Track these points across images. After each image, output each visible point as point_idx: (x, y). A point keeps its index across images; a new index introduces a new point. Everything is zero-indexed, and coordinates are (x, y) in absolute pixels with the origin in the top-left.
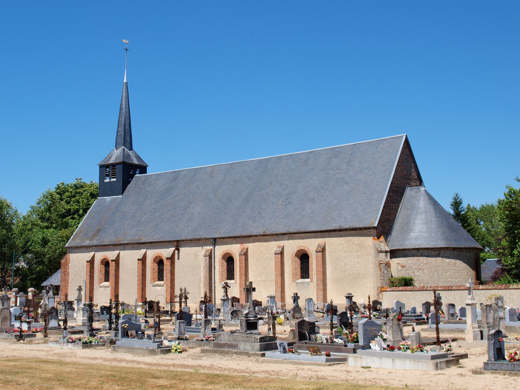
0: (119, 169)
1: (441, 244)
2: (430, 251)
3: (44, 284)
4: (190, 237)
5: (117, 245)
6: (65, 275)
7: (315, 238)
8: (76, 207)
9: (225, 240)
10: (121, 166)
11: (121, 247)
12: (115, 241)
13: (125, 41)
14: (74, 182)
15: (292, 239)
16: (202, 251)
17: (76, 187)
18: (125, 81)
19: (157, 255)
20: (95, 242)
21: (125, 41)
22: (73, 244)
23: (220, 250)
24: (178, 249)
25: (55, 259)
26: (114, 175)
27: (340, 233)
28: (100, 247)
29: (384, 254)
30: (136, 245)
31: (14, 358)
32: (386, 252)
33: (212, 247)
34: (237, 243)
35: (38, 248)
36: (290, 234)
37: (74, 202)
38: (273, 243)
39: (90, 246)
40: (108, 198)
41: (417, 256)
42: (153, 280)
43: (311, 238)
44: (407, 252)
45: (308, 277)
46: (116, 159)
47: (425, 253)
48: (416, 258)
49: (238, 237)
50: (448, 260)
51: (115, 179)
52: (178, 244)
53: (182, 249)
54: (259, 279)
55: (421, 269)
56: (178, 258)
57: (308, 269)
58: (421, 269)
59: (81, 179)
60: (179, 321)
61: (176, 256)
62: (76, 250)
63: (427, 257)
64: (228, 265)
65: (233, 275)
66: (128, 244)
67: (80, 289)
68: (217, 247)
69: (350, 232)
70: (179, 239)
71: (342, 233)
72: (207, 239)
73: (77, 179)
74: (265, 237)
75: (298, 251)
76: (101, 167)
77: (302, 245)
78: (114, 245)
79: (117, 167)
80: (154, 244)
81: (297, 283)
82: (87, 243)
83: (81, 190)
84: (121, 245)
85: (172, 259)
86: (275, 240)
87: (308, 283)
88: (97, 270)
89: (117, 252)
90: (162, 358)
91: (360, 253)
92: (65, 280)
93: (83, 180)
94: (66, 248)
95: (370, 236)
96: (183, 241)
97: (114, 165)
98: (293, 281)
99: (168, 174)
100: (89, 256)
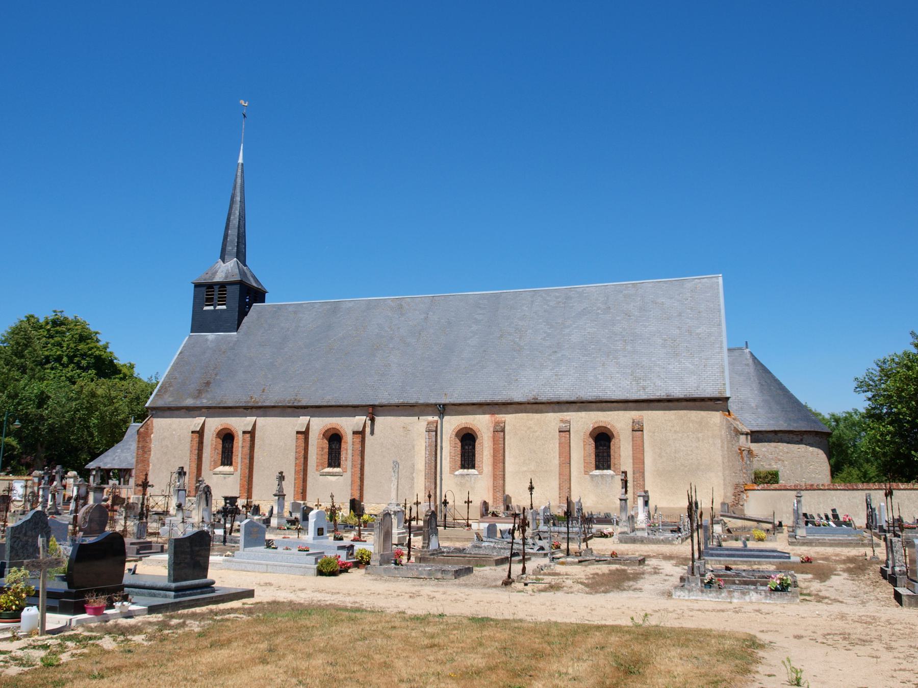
0: (233, 293)
1: (782, 426)
2: (791, 436)
3: (92, 465)
4: (395, 401)
5: (252, 408)
6: (144, 452)
7: (625, 409)
8: (58, 353)
9: (461, 408)
10: (238, 287)
11: (258, 411)
12: (248, 402)
13: (242, 102)
14: (51, 316)
15: (585, 410)
16: (419, 425)
17: (55, 323)
18: (240, 161)
19: (329, 427)
20: (204, 402)
21: (242, 102)
22: (160, 403)
23: (452, 424)
24: (373, 420)
25: (61, 427)
26: (222, 300)
27: (667, 404)
28: (217, 410)
29: (744, 436)
30: (290, 410)
31: (357, 605)
32: (747, 434)
33: (436, 418)
34: (484, 413)
35: (32, 409)
36: (582, 402)
37: (53, 345)
38: (551, 415)
39: (197, 408)
40: (211, 336)
41: (774, 442)
42: (320, 465)
43: (618, 410)
44: (760, 436)
45: (473, 467)
46: (226, 277)
47: (786, 437)
48: (773, 444)
49: (488, 404)
50: (811, 449)
51: (224, 307)
52: (373, 411)
53: (379, 420)
54: (525, 469)
55: (779, 460)
56: (372, 433)
57: (474, 455)
58: (779, 460)
59: (62, 312)
60: (440, 529)
61: (368, 430)
62: (168, 413)
63: (788, 443)
64: (462, 446)
65: (609, 456)
66: (274, 407)
67: (281, 477)
68: (446, 418)
69: (684, 404)
70: (377, 403)
71: (670, 404)
72: (428, 405)
73: (55, 311)
74: (535, 406)
75: (595, 429)
76: (197, 286)
77: (602, 419)
78: (246, 408)
79: (228, 287)
80: (325, 409)
81: (592, 476)
82: (189, 402)
83: (63, 328)
84: (260, 407)
85: (360, 434)
86: (554, 412)
87: (612, 476)
88: (209, 447)
89: (252, 419)
90: (630, 598)
91: (700, 435)
92: (143, 461)
93: (66, 314)
94: (147, 408)
95: (717, 411)
96: (382, 406)
97: (223, 285)
98: (586, 472)
99: (316, 306)
100: (196, 422)
